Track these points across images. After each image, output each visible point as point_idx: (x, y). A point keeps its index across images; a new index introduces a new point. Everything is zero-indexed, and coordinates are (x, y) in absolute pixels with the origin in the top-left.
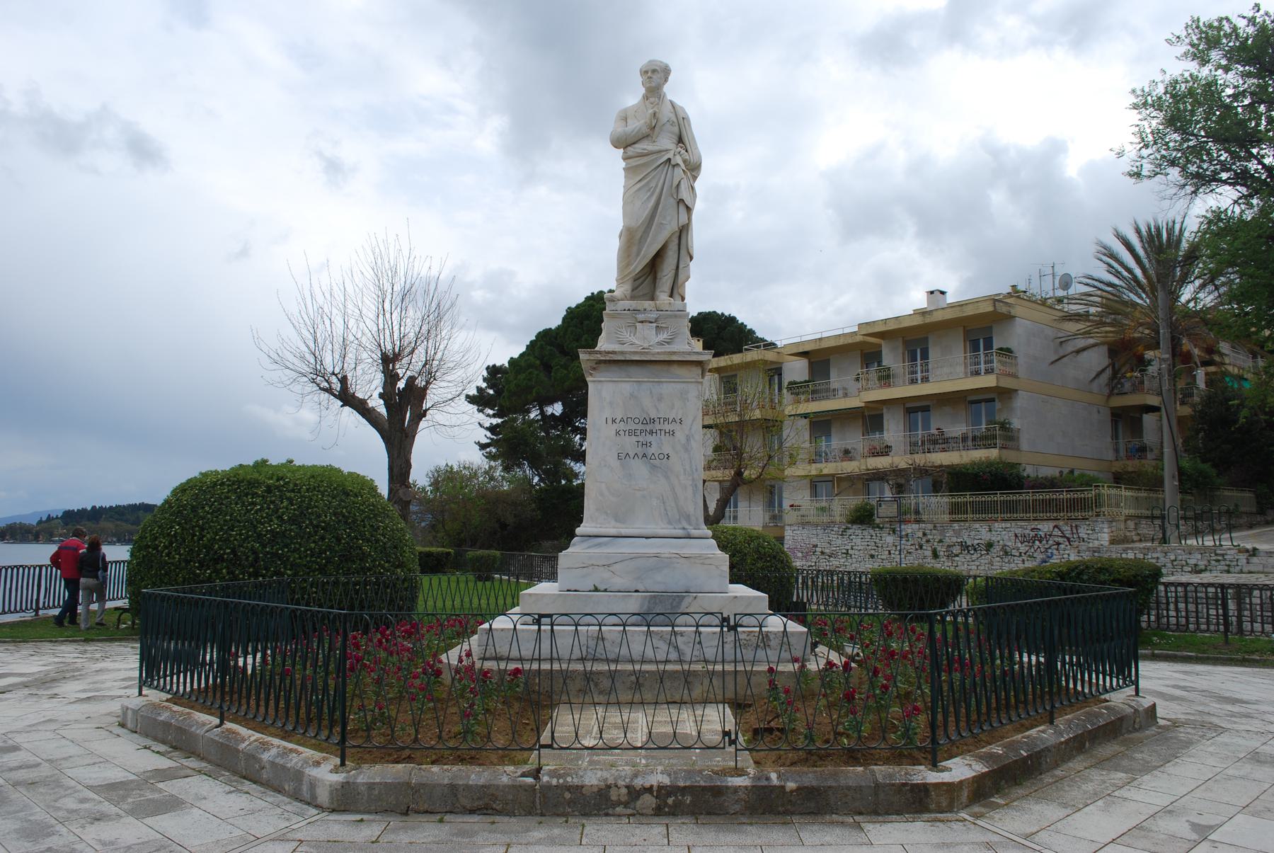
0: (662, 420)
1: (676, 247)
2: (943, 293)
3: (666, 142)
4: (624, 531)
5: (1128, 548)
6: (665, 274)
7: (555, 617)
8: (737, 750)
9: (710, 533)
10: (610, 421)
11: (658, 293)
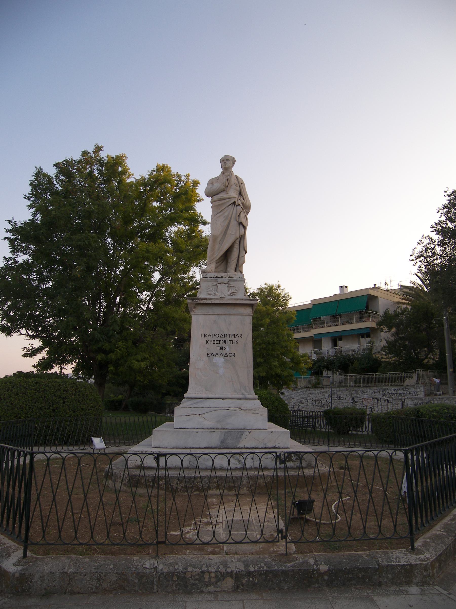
0: (231, 335)
1: (238, 246)
2: (346, 287)
3: (233, 193)
4: (210, 396)
5: (434, 398)
6: (232, 260)
7: (168, 456)
8: (287, 543)
9: (257, 396)
10: (203, 336)
11: (228, 269)
